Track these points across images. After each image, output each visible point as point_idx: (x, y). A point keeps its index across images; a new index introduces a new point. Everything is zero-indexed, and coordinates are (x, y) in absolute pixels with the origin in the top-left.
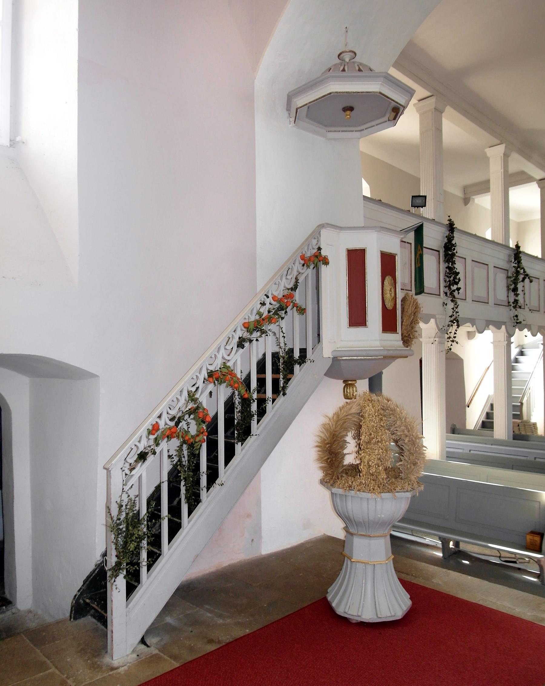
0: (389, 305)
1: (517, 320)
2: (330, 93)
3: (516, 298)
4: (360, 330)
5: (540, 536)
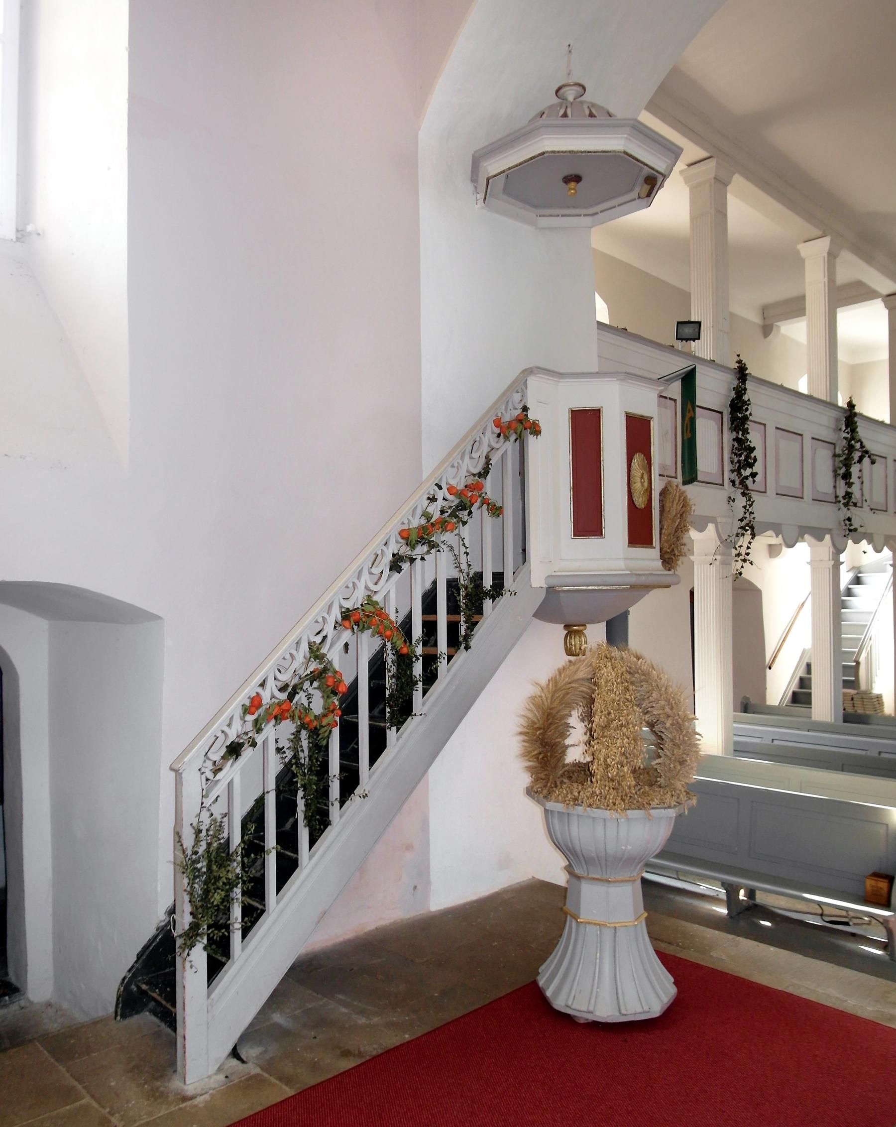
0: (640, 502)
1: (851, 525)
2: (543, 153)
3: (849, 490)
4: (591, 542)
5: (887, 881)
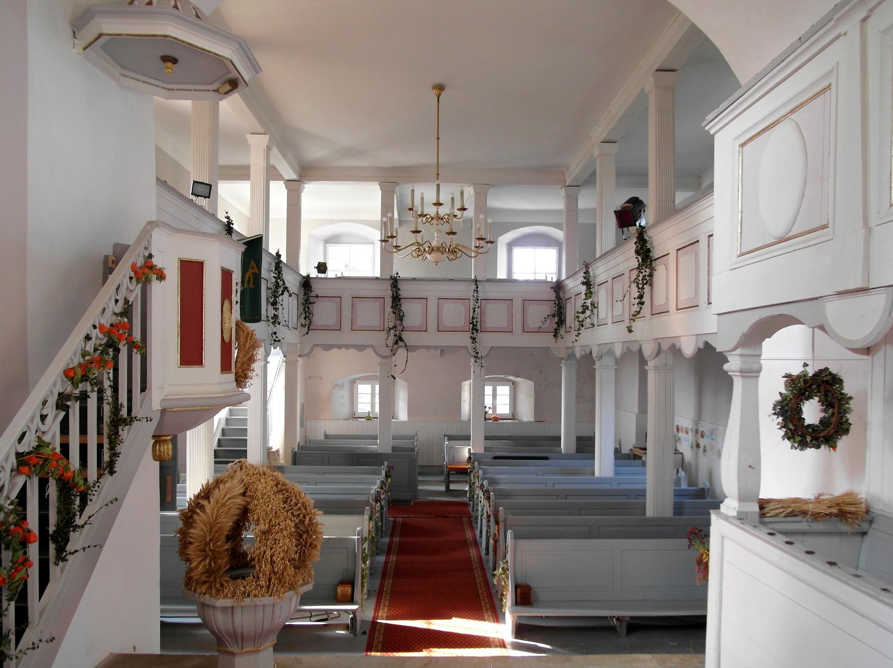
0: (227, 339)
1: (277, 337)
2: (166, 36)
3: (276, 313)
4: (193, 370)
5: (351, 585)
